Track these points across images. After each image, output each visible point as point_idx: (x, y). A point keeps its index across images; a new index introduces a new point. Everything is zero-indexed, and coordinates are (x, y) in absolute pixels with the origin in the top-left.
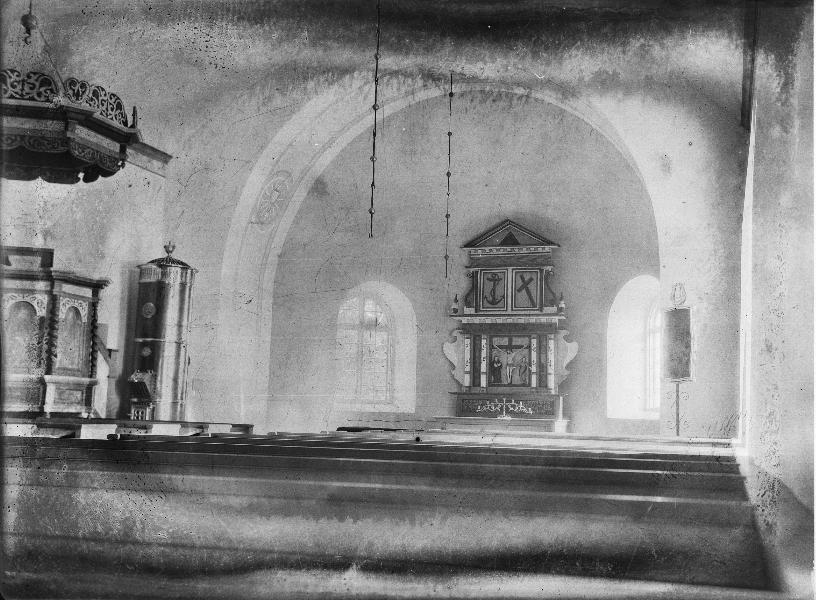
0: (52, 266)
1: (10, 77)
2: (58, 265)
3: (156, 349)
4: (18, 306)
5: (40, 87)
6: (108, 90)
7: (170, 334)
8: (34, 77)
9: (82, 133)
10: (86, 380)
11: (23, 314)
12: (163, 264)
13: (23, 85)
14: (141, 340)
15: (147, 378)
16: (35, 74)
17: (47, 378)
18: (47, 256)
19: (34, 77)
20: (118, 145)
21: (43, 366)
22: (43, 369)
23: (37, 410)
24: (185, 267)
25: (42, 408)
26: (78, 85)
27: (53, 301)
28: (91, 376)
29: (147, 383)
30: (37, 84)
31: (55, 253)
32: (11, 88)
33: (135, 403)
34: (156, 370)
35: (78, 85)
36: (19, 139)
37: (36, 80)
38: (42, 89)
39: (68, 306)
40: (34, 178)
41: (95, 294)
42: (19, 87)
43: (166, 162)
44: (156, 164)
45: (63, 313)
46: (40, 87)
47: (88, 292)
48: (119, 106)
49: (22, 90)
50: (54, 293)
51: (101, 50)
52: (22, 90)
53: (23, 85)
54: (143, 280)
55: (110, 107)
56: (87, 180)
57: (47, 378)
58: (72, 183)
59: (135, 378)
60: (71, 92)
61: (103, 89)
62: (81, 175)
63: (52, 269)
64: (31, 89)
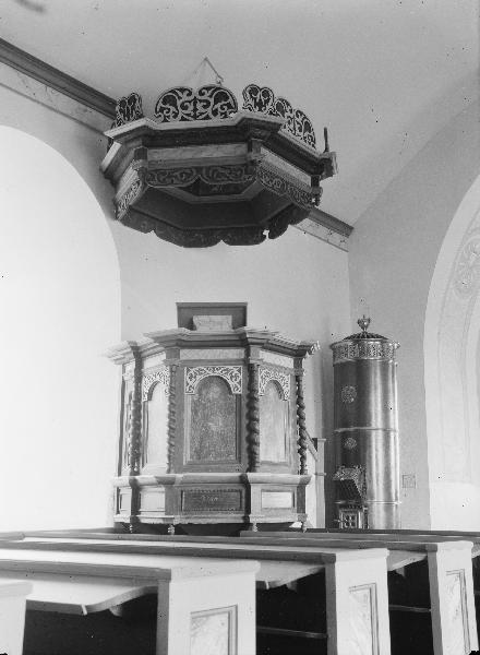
0: (244, 324)
1: (180, 98)
2: (255, 324)
3: (363, 440)
4: (206, 383)
5: (216, 103)
6: (294, 107)
7: (376, 420)
8: (207, 94)
9: (270, 158)
10: (298, 477)
11: (215, 392)
12: (357, 339)
13: (195, 105)
14: (340, 430)
15: (355, 475)
16: (208, 89)
17: (250, 476)
18: (239, 313)
19: (207, 94)
20: (309, 178)
21: (245, 460)
22: (245, 463)
23: (242, 521)
24: (383, 340)
25: (246, 518)
26: (260, 93)
27: (250, 370)
28: (302, 472)
29: (356, 482)
30: (212, 100)
31: (249, 307)
32: (180, 110)
33: (341, 506)
34: (364, 466)
35: (260, 93)
36: (194, 170)
37: (211, 96)
38: (218, 106)
39: (268, 379)
40: (215, 242)
41: (298, 365)
42: (191, 107)
43: (347, 235)
44: (337, 237)
45: (262, 385)
46: (216, 103)
47: (288, 362)
48: (308, 127)
49: (195, 110)
50: (251, 362)
51: (240, 354)
52: (195, 110)
53: (195, 105)
54: (339, 361)
55: (297, 126)
56: (272, 236)
57: (250, 476)
58: (257, 242)
59: (341, 475)
60: (251, 102)
61: (288, 104)
62: (266, 233)
63: (246, 328)
64: (204, 107)
